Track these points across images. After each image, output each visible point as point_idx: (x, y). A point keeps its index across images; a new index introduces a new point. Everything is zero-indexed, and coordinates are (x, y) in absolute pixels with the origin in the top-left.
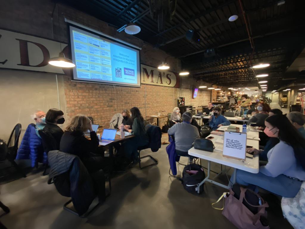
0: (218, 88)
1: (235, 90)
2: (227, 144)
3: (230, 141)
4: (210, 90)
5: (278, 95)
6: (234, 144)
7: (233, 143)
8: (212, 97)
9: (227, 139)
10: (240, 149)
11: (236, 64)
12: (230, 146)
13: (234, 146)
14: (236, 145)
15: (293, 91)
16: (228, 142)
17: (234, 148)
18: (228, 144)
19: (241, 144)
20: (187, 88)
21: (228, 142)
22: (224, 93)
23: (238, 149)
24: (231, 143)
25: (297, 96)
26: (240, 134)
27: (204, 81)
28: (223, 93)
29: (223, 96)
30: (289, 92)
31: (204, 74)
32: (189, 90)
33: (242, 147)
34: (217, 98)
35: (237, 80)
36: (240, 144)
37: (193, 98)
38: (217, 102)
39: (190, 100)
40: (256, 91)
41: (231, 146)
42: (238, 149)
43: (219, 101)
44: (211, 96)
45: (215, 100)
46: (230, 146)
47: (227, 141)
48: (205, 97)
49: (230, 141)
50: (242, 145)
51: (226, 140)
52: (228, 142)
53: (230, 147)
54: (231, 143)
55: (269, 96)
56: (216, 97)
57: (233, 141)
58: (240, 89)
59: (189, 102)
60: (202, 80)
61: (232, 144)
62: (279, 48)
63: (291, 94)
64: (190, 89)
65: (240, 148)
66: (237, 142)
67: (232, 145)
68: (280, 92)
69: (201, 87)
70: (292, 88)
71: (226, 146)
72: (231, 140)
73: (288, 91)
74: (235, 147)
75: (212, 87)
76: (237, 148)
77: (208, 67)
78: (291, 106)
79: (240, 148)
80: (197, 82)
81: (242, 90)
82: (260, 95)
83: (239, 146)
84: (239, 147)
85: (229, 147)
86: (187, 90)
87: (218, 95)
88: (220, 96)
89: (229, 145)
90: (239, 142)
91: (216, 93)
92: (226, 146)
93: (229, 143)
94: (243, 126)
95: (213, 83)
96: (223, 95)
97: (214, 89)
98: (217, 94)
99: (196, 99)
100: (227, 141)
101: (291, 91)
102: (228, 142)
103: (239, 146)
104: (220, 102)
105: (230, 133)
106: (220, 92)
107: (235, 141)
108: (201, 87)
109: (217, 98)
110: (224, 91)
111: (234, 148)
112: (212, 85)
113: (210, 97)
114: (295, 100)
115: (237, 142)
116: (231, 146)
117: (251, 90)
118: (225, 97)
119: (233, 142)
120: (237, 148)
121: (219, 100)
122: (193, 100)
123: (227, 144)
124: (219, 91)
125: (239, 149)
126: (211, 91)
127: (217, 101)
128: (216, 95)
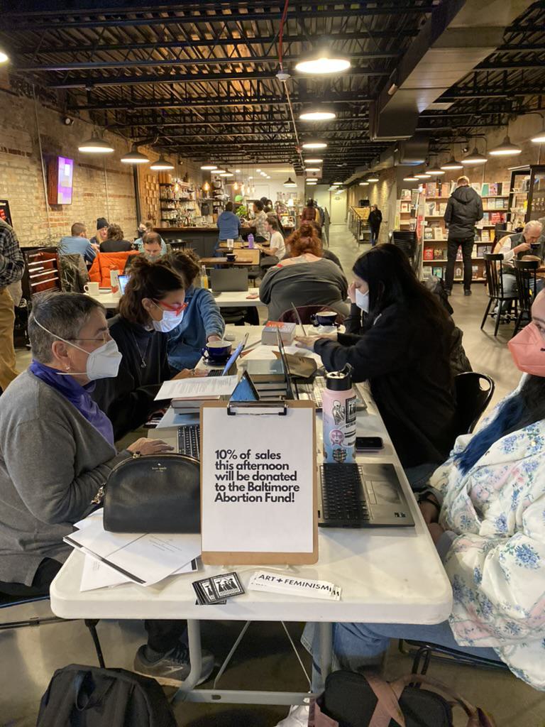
0: (162, 161)
1: (223, 173)
2: (220, 483)
3: (235, 462)
4: (129, 165)
5: (343, 200)
6: (258, 477)
7: (252, 473)
8: (143, 202)
9: (219, 453)
10: (289, 499)
11: (212, 52)
12: (237, 493)
13: (255, 489)
14: (266, 477)
15: (385, 185)
16: (226, 467)
17: (256, 499)
18: (226, 483)
19: (290, 473)
20: (14, 148)
21: (223, 472)
22: (188, 185)
23: (278, 499)
24: (243, 472)
25: (402, 202)
26: (284, 413)
27: (95, 119)
28: (182, 188)
29: (183, 200)
30: (375, 189)
31: (90, 79)
32: (25, 161)
33: (296, 488)
34: (162, 210)
35: (229, 129)
36: (285, 472)
37: (55, 206)
38: (165, 225)
39: (42, 213)
40: (290, 181)
41: (240, 488)
42: (278, 499)
43: (172, 221)
44: (137, 197)
45: (157, 216)
46: (237, 493)
47: (219, 466)
48: (110, 201)
49: (235, 462)
50: (294, 477)
51: (215, 459)
52: (223, 472)
53: (238, 499)
54: (243, 472)
55: (322, 201)
56: (158, 202)
57: (252, 460)
58: (238, 171)
59: (36, 227)
60: (85, 114)
61: (244, 478)
62: (337, 7)
63: (381, 195)
64: (29, 155)
65: (286, 494)
66: (269, 461)
67: (245, 483)
68: (352, 187)
69: (85, 149)
70: (382, 175)
71: (218, 498)
72: (238, 453)
73: (371, 185)
74: (263, 494)
75: (135, 154)
76: (274, 494)
77: (108, 46)
78: (390, 235)
79: (286, 494)
80: (63, 120)
81: (246, 176)
82: (298, 199)
83: (281, 483)
84: (281, 488)
85: (230, 499)
86: (16, 161)
87: (164, 195)
88: (171, 201)
89: (232, 487)
90: (281, 462)
91: (157, 186)
92: (218, 498)
93: (230, 476)
94: (154, 330)
95: (139, 136)
96: (186, 195)
97: (146, 166)
98: (160, 191)
99: (70, 213)
100: (219, 466)
101: (380, 185)
102: (226, 467)
103: (281, 483)
104: (175, 226)
105: (230, 413)
106: (171, 180)
107: (258, 456)
108: (85, 149)
109: (162, 210)
110: (185, 180)
111: (256, 499)
112: (137, 144)
113: (134, 200)
114: (398, 215)
115: (269, 461)
116: (240, 488)
117: (275, 179)
118: (191, 206)
119: (252, 467)
120: (274, 494)
121: (173, 216)
122: (56, 215)
123: (220, 483)
124: (165, 173)
125: (284, 499)
126: (134, 172)
127: (163, 220)
128: (156, 195)
